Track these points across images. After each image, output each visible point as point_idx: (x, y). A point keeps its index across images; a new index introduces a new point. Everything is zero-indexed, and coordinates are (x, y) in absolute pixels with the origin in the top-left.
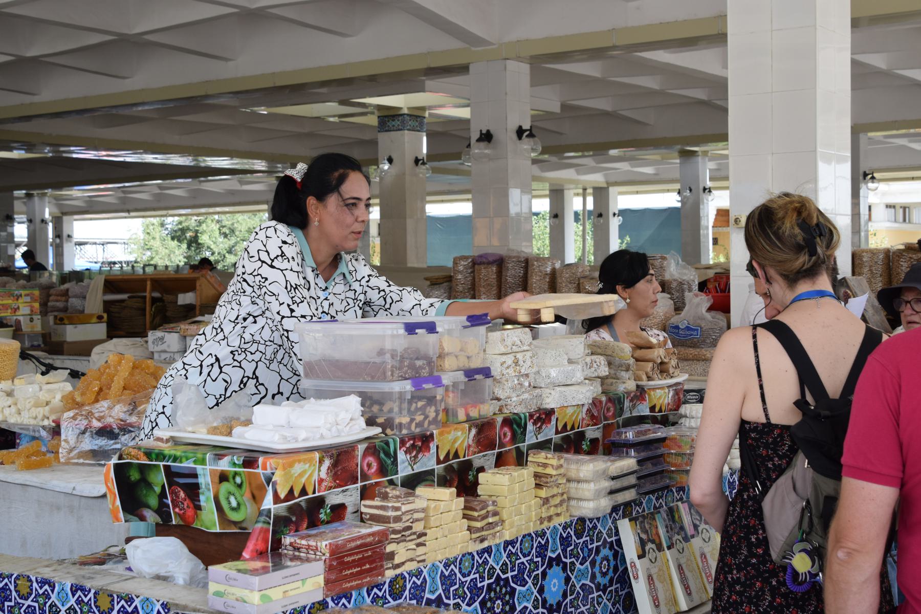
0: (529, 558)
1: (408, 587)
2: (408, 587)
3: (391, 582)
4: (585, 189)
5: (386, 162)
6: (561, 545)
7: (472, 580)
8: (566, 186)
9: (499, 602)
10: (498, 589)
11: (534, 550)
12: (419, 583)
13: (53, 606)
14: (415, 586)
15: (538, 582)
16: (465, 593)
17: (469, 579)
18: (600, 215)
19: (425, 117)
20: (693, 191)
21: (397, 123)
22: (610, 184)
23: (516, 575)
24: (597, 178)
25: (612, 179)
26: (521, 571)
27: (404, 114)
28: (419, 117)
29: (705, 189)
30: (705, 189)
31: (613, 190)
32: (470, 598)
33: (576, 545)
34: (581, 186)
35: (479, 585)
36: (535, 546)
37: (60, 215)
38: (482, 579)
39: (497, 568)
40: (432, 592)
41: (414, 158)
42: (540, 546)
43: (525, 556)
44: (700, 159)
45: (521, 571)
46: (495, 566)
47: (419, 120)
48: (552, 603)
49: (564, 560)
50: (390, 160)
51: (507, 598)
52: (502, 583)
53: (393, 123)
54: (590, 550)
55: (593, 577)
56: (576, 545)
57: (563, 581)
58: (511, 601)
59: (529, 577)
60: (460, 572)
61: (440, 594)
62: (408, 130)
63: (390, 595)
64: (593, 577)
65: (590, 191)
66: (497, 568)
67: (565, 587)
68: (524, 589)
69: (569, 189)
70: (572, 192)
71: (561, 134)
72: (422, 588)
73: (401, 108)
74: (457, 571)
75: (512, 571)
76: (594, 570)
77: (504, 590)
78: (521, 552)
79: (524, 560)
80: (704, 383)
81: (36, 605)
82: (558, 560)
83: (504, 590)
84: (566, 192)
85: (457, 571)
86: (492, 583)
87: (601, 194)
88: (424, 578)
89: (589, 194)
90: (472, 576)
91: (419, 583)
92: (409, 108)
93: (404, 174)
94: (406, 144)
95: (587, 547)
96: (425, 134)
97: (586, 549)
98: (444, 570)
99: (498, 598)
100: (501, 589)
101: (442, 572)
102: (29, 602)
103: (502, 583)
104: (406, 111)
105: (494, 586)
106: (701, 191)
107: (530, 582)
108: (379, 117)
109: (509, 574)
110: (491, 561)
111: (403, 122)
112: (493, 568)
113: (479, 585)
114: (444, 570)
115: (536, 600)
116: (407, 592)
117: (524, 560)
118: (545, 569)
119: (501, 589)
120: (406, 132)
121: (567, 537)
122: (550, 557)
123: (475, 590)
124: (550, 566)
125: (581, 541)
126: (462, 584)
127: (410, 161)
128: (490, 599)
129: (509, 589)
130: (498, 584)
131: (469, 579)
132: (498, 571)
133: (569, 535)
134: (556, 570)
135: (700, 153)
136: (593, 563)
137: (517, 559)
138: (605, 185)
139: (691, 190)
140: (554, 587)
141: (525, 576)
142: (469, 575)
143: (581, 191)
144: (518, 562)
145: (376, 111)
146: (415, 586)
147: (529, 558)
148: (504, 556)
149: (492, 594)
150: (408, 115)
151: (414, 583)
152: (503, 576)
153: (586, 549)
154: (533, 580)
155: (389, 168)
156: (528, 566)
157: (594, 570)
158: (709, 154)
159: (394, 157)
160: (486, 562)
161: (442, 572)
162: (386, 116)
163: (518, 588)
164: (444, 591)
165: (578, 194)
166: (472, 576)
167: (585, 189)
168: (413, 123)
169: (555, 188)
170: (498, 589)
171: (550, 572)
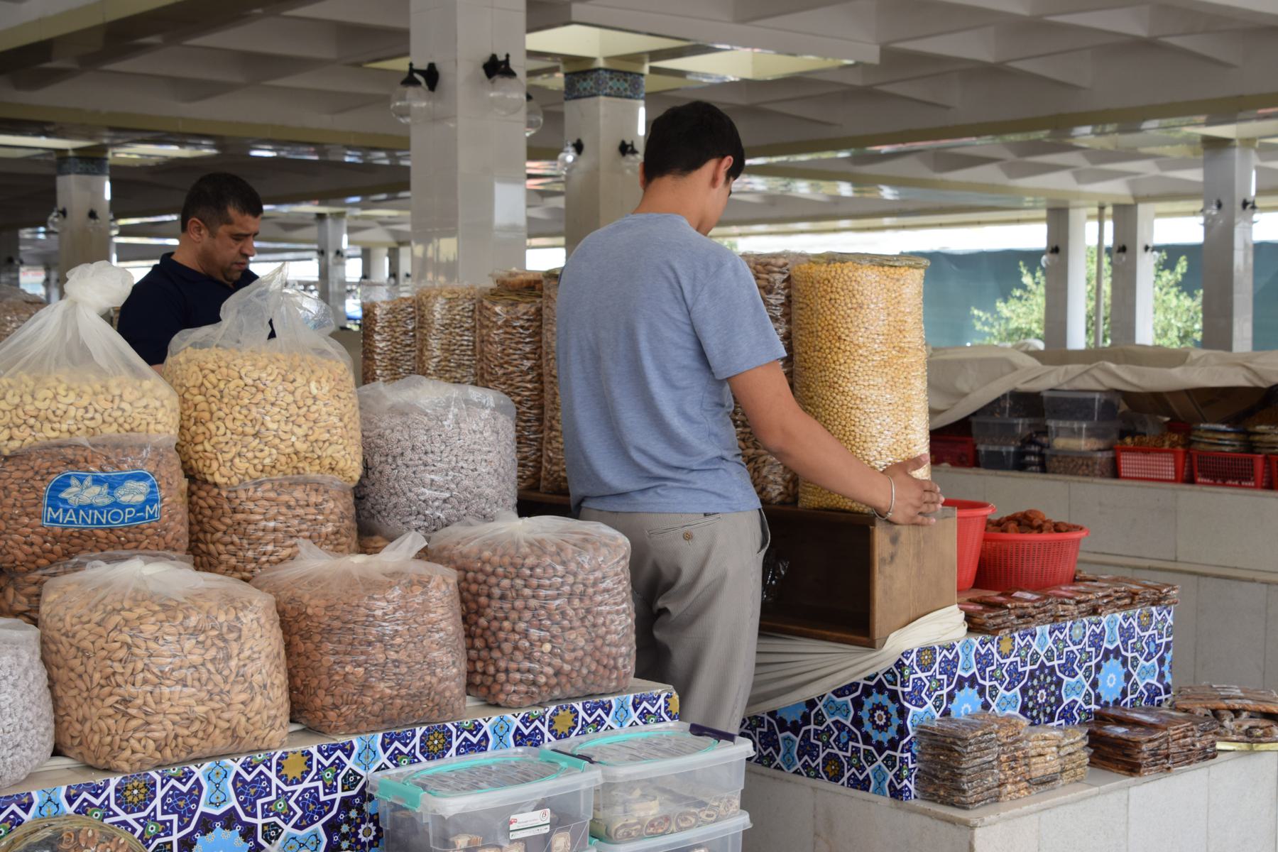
0: (1080, 647)
1: (938, 660)
2: (938, 660)
3: (918, 651)
4: (1102, 208)
5: (571, 149)
6: (1121, 636)
7: (1011, 663)
8: (1073, 203)
9: (1043, 691)
10: (1042, 677)
11: (1086, 639)
12: (950, 657)
13: (276, 831)
14: (946, 660)
15: (1090, 675)
16: (1003, 676)
17: (1008, 661)
18: (1123, 249)
19: (642, 75)
20: (1225, 206)
21: (589, 84)
22: (1139, 199)
23: (1063, 665)
24: (1117, 189)
25: (1143, 191)
26: (1070, 660)
27: (599, 69)
28: (631, 73)
29: (1245, 204)
30: (1245, 204)
31: (1143, 209)
32: (1009, 683)
33: (1140, 638)
34: (1096, 203)
35: (1020, 670)
36: (1088, 634)
37: (395, 245)
38: (1024, 663)
39: (1042, 653)
40: (966, 670)
41: (618, 143)
42: (1094, 634)
43: (1075, 644)
44: (1237, 152)
45: (1070, 660)
46: (1039, 651)
47: (629, 78)
48: (1108, 700)
49: (1124, 653)
50: (579, 147)
51: (1053, 688)
52: (1046, 671)
53: (585, 84)
54: (1159, 646)
55: (1162, 675)
56: (1140, 638)
57: (1100, 684)
58: (1057, 693)
59: (1080, 668)
60: (999, 653)
61: (974, 674)
62: (606, 95)
63: (918, 666)
64: (1162, 675)
65: (1109, 211)
66: (1042, 653)
67: (1125, 685)
68: (1073, 680)
69: (1078, 207)
70: (1084, 213)
71: (948, 108)
72: (954, 663)
73: (592, 60)
74: (994, 650)
75: (1059, 658)
76: (1163, 669)
77: (1049, 679)
78: (1071, 640)
79: (1074, 648)
80: (760, 661)
81: (273, 797)
82: (1116, 652)
83: (1049, 679)
84: (1073, 214)
85: (994, 650)
86: (1036, 670)
87: (1125, 215)
88: (957, 653)
89: (1108, 216)
90: (1012, 659)
91: (950, 657)
92: (607, 59)
93: (598, 169)
94: (602, 121)
95: (1154, 641)
96: (642, 102)
97: (1152, 645)
98: (980, 648)
99: (1041, 687)
100: (1045, 678)
101: (977, 650)
102: (275, 781)
103: (1046, 671)
104: (601, 64)
105: (1038, 673)
106: (1238, 206)
107: (1081, 674)
108: (566, 75)
109: (1056, 663)
110: (1035, 646)
111: (597, 83)
112: (1037, 653)
113: (1020, 670)
114: (980, 648)
115: (1134, 667)
116: (936, 665)
117: (1074, 648)
118: (1100, 661)
119: (1045, 678)
120: (602, 98)
121: (1128, 628)
122: (1106, 649)
123: (1015, 675)
124: (1106, 658)
125: (1147, 634)
126: (1000, 666)
127: (608, 146)
128: (1033, 687)
129: (1054, 679)
130: (1042, 672)
131: (1008, 661)
132: (1043, 658)
133: (1131, 627)
134: (1114, 663)
135: (1237, 143)
136: (1161, 661)
137: (1065, 647)
138: (1131, 201)
139: (1219, 206)
140: (1112, 679)
141: (1075, 666)
142: (1008, 657)
143: (1095, 211)
144: (1066, 650)
145: (562, 67)
146: (946, 660)
147: (1080, 647)
148: (1050, 642)
149: (1035, 682)
150: (606, 70)
151: (945, 656)
152: (1048, 664)
153: (1152, 645)
154: (1085, 671)
155: (575, 160)
156: (1079, 656)
157: (1163, 669)
158: (1257, 145)
159: (585, 141)
160: (1029, 646)
161: (977, 650)
162: (575, 73)
163: (1066, 679)
164: (979, 670)
165: (1090, 217)
166: (1012, 659)
167: (1102, 208)
168: (618, 85)
169: (1053, 205)
170: (1042, 677)
171: (1106, 665)
